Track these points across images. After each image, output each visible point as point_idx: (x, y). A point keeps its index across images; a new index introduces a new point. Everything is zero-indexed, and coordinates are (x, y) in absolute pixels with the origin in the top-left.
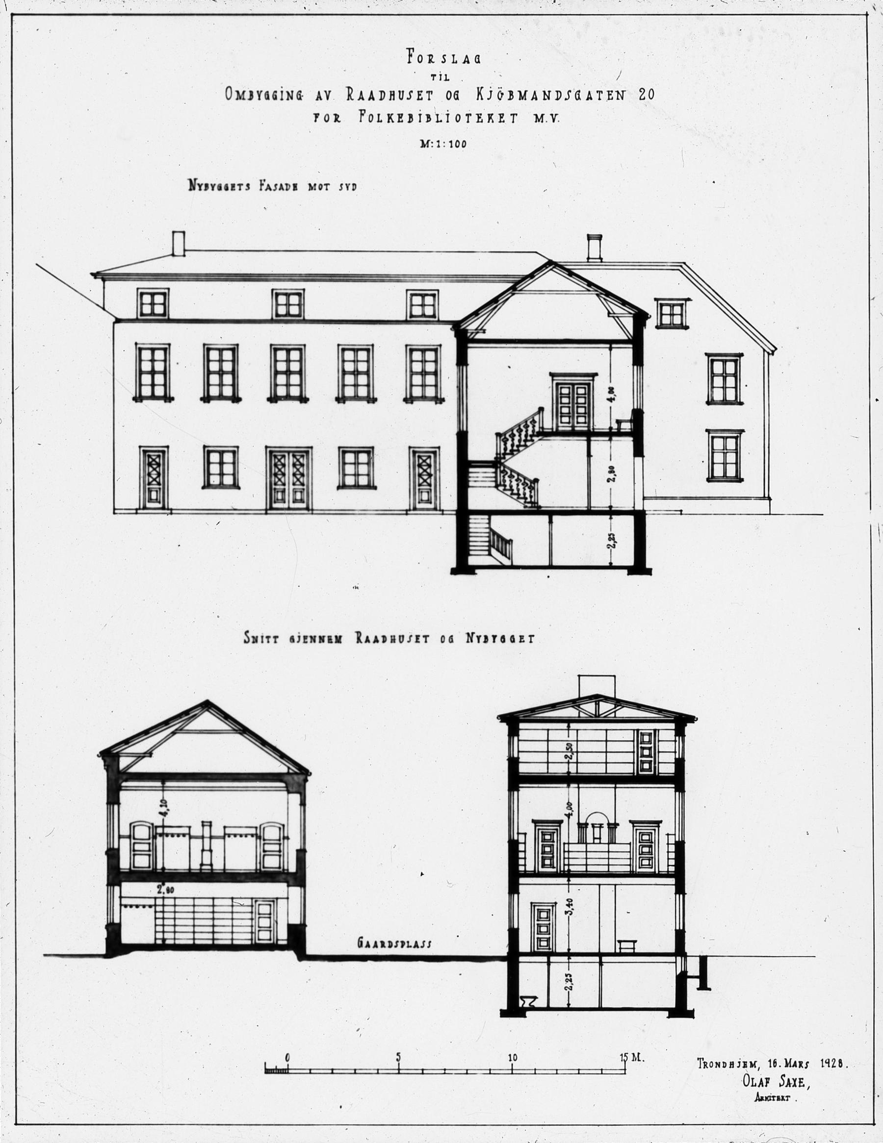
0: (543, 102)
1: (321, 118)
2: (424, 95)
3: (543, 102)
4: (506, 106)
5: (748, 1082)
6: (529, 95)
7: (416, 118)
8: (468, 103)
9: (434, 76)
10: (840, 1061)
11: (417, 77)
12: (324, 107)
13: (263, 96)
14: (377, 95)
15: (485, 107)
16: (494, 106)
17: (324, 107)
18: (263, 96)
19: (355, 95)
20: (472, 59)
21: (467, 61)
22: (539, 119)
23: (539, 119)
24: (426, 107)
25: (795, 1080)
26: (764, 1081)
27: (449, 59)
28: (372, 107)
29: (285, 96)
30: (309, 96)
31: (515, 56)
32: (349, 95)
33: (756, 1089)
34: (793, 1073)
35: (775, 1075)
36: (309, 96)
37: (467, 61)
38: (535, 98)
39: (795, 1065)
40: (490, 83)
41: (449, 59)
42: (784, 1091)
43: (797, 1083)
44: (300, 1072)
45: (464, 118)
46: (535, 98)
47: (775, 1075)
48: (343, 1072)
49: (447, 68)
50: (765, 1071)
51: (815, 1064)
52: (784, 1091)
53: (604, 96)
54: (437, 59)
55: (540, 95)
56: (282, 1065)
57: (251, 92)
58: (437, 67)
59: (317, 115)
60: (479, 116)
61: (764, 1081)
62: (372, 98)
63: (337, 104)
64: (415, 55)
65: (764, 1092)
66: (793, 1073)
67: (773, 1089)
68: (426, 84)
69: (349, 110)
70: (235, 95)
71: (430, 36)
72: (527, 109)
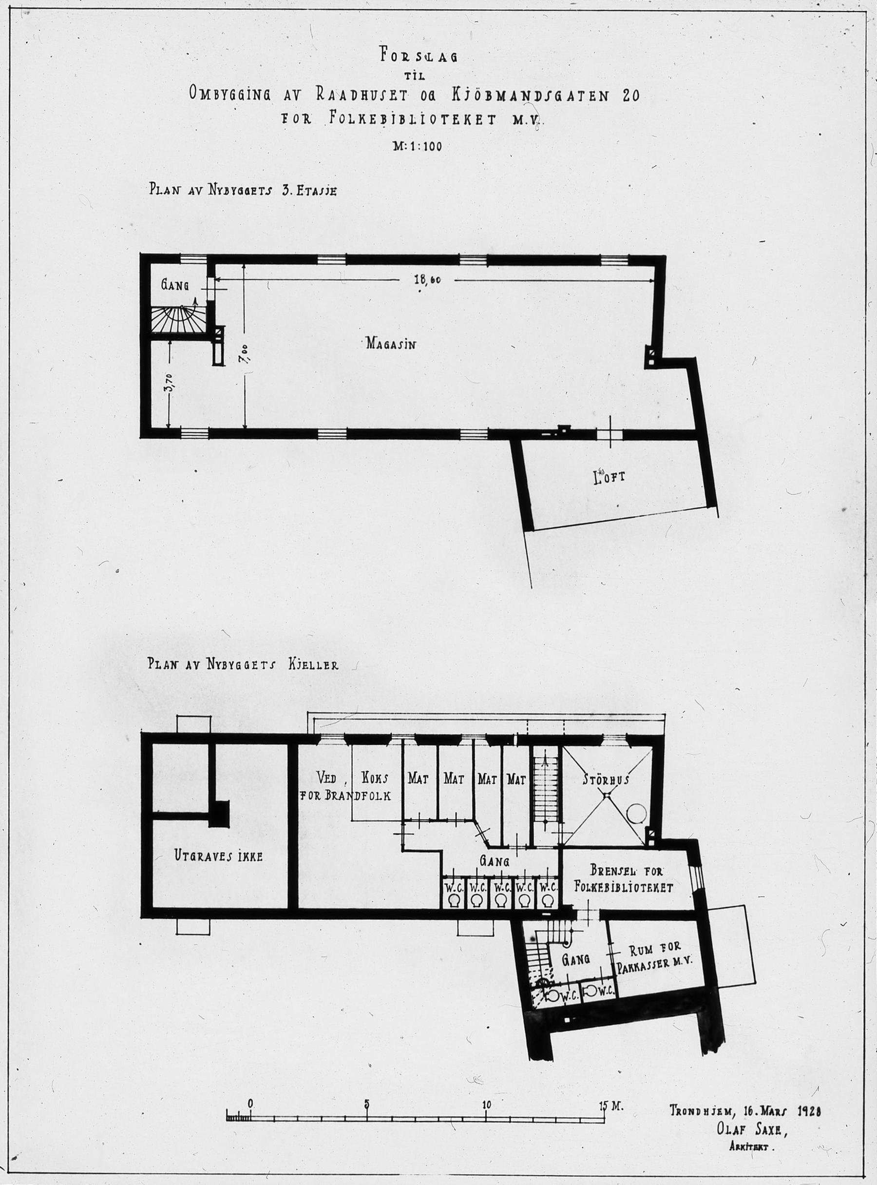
0: (526, 103)
3: (526, 103)
4: (484, 107)
6: (508, 96)
7: (389, 119)
8: (444, 104)
9: (408, 74)
10: (819, 1109)
11: (390, 76)
15: (461, 108)
16: (472, 107)
17: (293, 108)
19: (326, 94)
20: (448, 57)
21: (443, 59)
23: (518, 121)
25: (771, 1128)
31: (498, 54)
34: (769, 1121)
35: (750, 1122)
36: (277, 95)
42: (762, 1139)
43: (774, 1130)
46: (514, 98)
47: (750, 1122)
49: (422, 66)
50: (740, 1119)
53: (586, 96)
54: (412, 57)
61: (739, 1129)
63: (307, 103)
64: (389, 53)
65: (739, 1140)
67: (749, 1137)
68: (401, 83)
69: (319, 111)
70: (199, 94)
72: (506, 110)
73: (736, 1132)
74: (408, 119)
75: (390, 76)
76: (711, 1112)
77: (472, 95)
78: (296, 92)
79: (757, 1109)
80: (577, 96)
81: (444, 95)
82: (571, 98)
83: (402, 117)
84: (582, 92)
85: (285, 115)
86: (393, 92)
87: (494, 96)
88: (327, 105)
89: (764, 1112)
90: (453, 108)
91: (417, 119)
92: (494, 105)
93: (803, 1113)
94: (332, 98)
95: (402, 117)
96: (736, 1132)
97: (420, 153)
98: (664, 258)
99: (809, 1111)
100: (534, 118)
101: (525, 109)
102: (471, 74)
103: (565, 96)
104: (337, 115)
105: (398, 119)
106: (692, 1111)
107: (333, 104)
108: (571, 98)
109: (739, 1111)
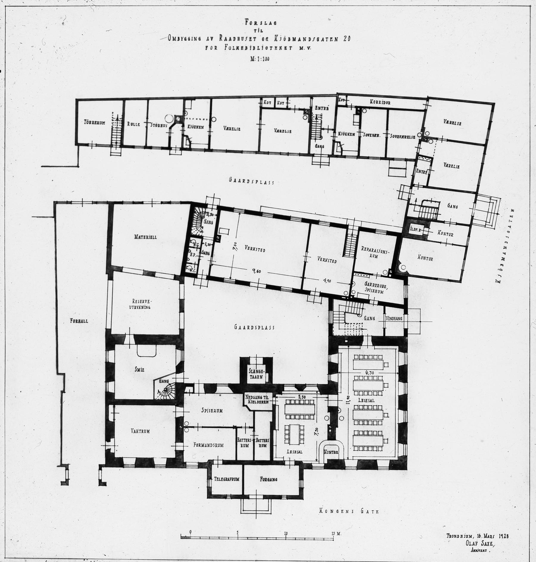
0: (302, 42)
1: (209, 48)
2: (253, 39)
3: (302, 42)
4: (287, 44)
5: (468, 544)
6: (297, 39)
7: (249, 48)
8: (271, 42)
9: (255, 30)
10: (508, 535)
11: (249, 31)
12: (210, 43)
13: (183, 39)
14: (232, 39)
15: (278, 44)
16: (283, 44)
17: (210, 43)
18: (183, 39)
19: (223, 38)
20: (273, 23)
21: (270, 24)
22: (301, 48)
23: (301, 48)
24: (253, 43)
25: (488, 543)
26: (475, 543)
27: (263, 23)
28: (231, 44)
29: (193, 39)
30: (204, 39)
31: (290, 23)
32: (220, 38)
33: (472, 546)
34: (487, 540)
35: (480, 541)
36: (204, 39)
37: (270, 24)
38: (299, 40)
39: (489, 537)
40: (282, 34)
41: (263, 23)
42: (484, 548)
43: (490, 544)
44: (196, 538)
45: (269, 48)
46: (299, 40)
47: (480, 541)
48: (223, 538)
49: (262, 27)
50: (476, 539)
51: (497, 536)
52: (484, 548)
53: (329, 39)
54: (259, 23)
55: (302, 39)
56: (188, 535)
57: (179, 38)
58: (258, 26)
59: (207, 47)
60: (276, 47)
61: (475, 543)
62: (230, 40)
63: (216, 42)
64: (249, 22)
65: (475, 548)
66: (487, 540)
67: (479, 547)
68: (253, 35)
69: (221, 45)
70: (172, 38)
71: (254, 15)
72: (296, 45)
73: (474, 545)
74: (256, 48)
75: (249, 31)
76: (464, 536)
77: (283, 39)
78: (212, 38)
79: (483, 536)
80: (325, 39)
81: (272, 38)
82: (323, 40)
83: (254, 47)
84: (327, 38)
85: (207, 47)
86: (250, 38)
87: (291, 39)
88: (223, 43)
89: (485, 537)
90: (275, 44)
91: (260, 48)
92: (292, 43)
93: (501, 537)
94: (226, 40)
95: (254, 47)
96: (474, 545)
97: (261, 62)
98: (76, 99)
99: (504, 536)
100: (309, 48)
101: (305, 44)
102: (282, 30)
103: (320, 39)
104: (228, 47)
105: (252, 48)
106: (455, 536)
107: (226, 42)
108: (323, 40)
109: (475, 535)
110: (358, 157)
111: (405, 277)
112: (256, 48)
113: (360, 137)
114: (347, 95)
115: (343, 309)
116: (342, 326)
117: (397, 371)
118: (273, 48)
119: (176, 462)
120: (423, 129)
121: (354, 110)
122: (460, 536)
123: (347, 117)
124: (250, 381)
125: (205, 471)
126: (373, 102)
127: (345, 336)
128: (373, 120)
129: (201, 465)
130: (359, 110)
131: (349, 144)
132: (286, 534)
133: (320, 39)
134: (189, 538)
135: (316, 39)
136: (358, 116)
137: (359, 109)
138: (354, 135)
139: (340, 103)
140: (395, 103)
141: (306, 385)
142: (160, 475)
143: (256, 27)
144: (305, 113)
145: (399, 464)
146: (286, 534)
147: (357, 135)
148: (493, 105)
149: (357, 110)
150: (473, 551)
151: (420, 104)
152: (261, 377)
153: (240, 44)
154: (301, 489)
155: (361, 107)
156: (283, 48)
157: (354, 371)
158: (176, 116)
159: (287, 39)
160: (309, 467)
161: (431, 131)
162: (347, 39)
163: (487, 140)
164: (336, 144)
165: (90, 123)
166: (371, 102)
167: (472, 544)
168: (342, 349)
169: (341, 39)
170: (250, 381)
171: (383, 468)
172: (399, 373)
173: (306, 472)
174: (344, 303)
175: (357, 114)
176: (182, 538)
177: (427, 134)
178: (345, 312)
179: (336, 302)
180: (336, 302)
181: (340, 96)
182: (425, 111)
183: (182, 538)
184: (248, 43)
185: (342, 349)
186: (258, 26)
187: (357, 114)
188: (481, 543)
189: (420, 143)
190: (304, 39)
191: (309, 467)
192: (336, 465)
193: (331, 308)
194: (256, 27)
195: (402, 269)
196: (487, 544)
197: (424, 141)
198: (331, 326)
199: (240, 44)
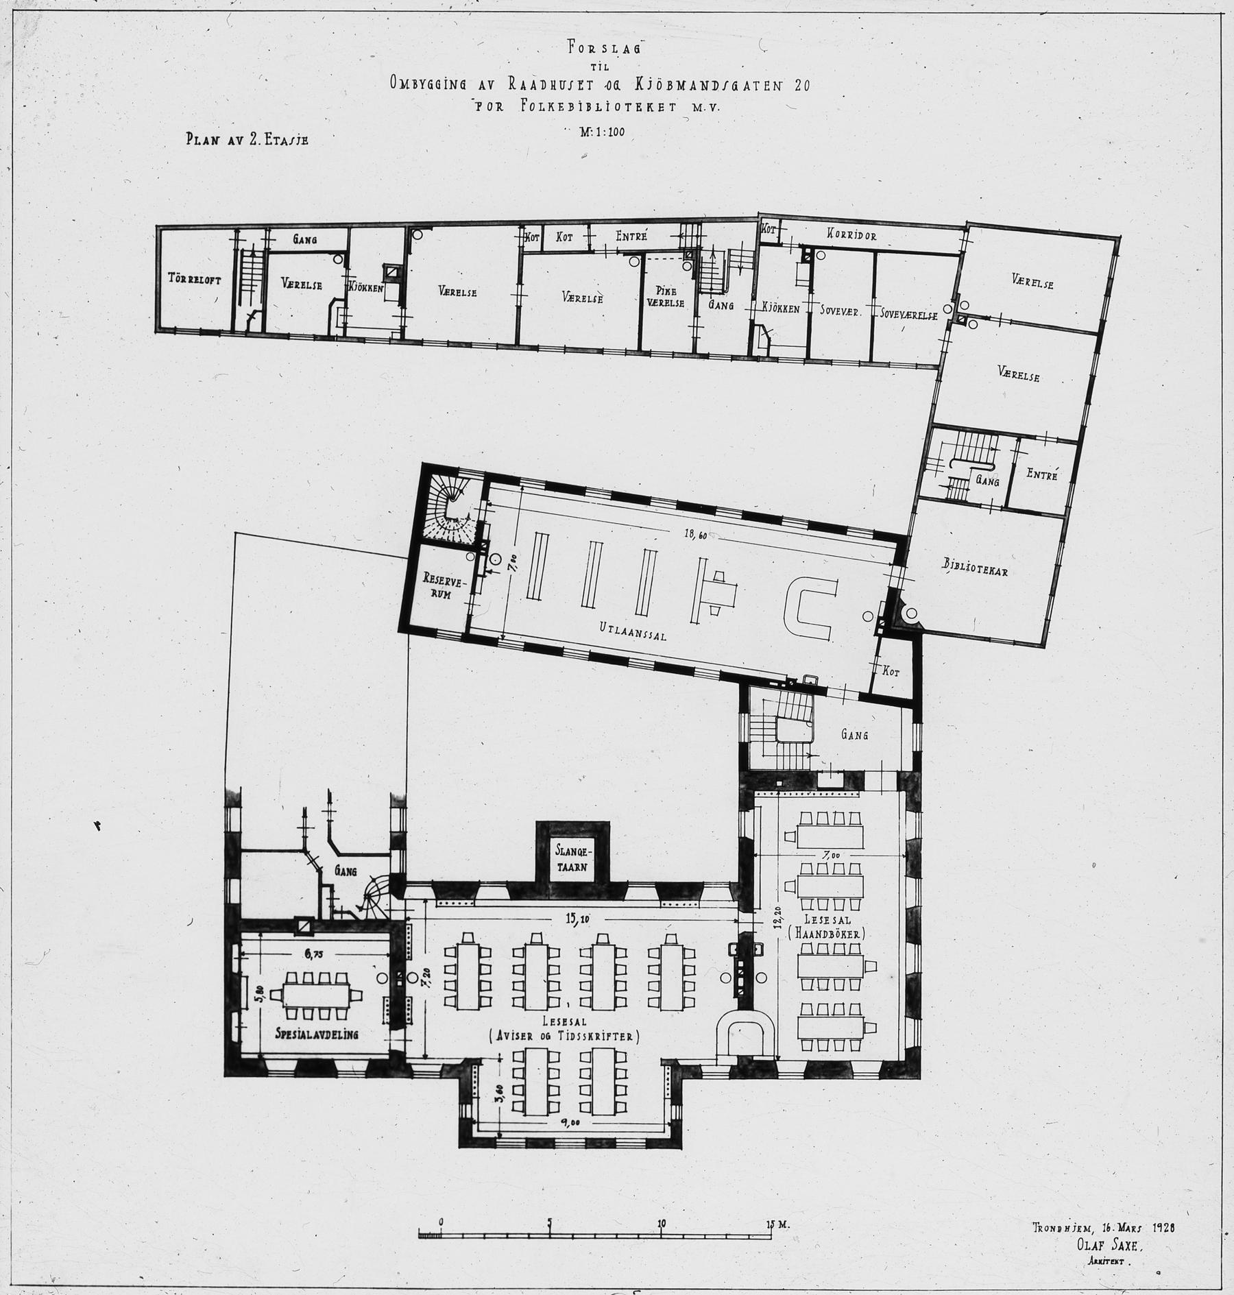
4: (665, 96)
5: (1082, 1246)
10: (1173, 1225)
11: (578, 67)
14: (539, 85)
15: (644, 97)
16: (655, 97)
17: (486, 96)
19: (518, 85)
22: (698, 108)
23: (698, 108)
24: (585, 97)
28: (533, 96)
30: (473, 86)
34: (1125, 1237)
35: (1108, 1238)
36: (473, 86)
42: (1118, 1255)
47: (1108, 1238)
49: (608, 58)
50: (1099, 1235)
53: (761, 86)
58: (597, 57)
60: (638, 105)
63: (500, 92)
65: (1098, 1255)
66: (1125, 1237)
67: (1106, 1253)
68: (587, 74)
69: (512, 100)
70: (399, 84)
71: (591, 31)
72: (685, 99)
74: (594, 107)
75: (578, 67)
81: (628, 84)
82: (747, 87)
91: (603, 106)
97: (605, 139)
102: (652, 65)
105: (585, 107)
107: (524, 94)
109: (1098, 1228)
110: (808, 360)
111: (915, 634)
112: (594, 107)
113: (810, 315)
114: (781, 218)
115: (771, 710)
116: (771, 748)
117: (756, 859)
118: (633, 107)
119: (393, 1066)
120: (956, 298)
121: (798, 253)
122: (1063, 1229)
123: (780, 266)
124: (556, 876)
125: (453, 1084)
126: (834, 234)
127: (777, 771)
128: (842, 276)
129: (448, 1071)
130: (809, 254)
131: (786, 332)
132: (662, 1223)
133: (741, 86)
134: (439, 1236)
135: (729, 86)
136: (808, 266)
137: (808, 251)
138: (797, 310)
139: (765, 238)
140: (886, 237)
141: (628, 883)
142: (351, 1093)
143: (594, 58)
144: (686, 258)
145: (908, 1066)
146: (662, 1223)
147: (804, 309)
148: (1117, 240)
149: (804, 254)
150: (1094, 1262)
151: (951, 241)
152: (584, 868)
153: (557, 96)
154: (676, 1126)
155: (813, 248)
156: (655, 107)
157: (800, 852)
158: (385, 266)
159: (665, 86)
160: (696, 1072)
161: (973, 302)
162: (802, 86)
163: (1103, 323)
164: (756, 328)
165: (183, 281)
166: (830, 235)
167: (1091, 1245)
168: (763, 799)
169: (789, 86)
170: (556, 876)
171: (790, 1075)
172: (907, 856)
173: (688, 1085)
174: (773, 694)
175: (804, 261)
176: (422, 1236)
177: (964, 305)
178: (777, 717)
179: (756, 693)
180: (756, 693)
181: (764, 221)
182: (961, 255)
183: (422, 1236)
184: (574, 96)
185: (763, 799)
186: (597, 57)
187: (804, 261)
188: (1110, 1246)
189: (949, 328)
190: (681, 86)
191: (696, 1072)
192: (752, 1068)
193: (744, 707)
194: (594, 58)
195: (908, 616)
196: (1125, 1246)
197: (959, 323)
198: (744, 749)
199: (557, 96)
